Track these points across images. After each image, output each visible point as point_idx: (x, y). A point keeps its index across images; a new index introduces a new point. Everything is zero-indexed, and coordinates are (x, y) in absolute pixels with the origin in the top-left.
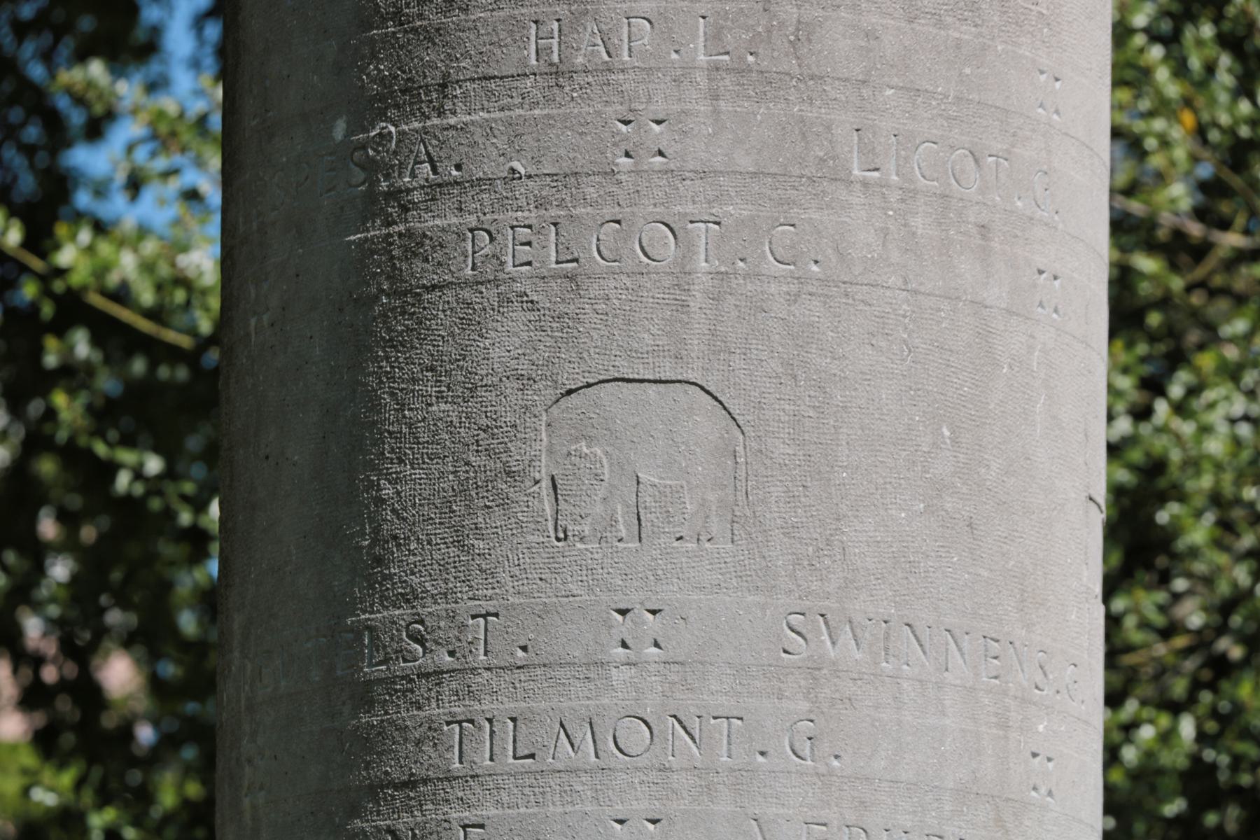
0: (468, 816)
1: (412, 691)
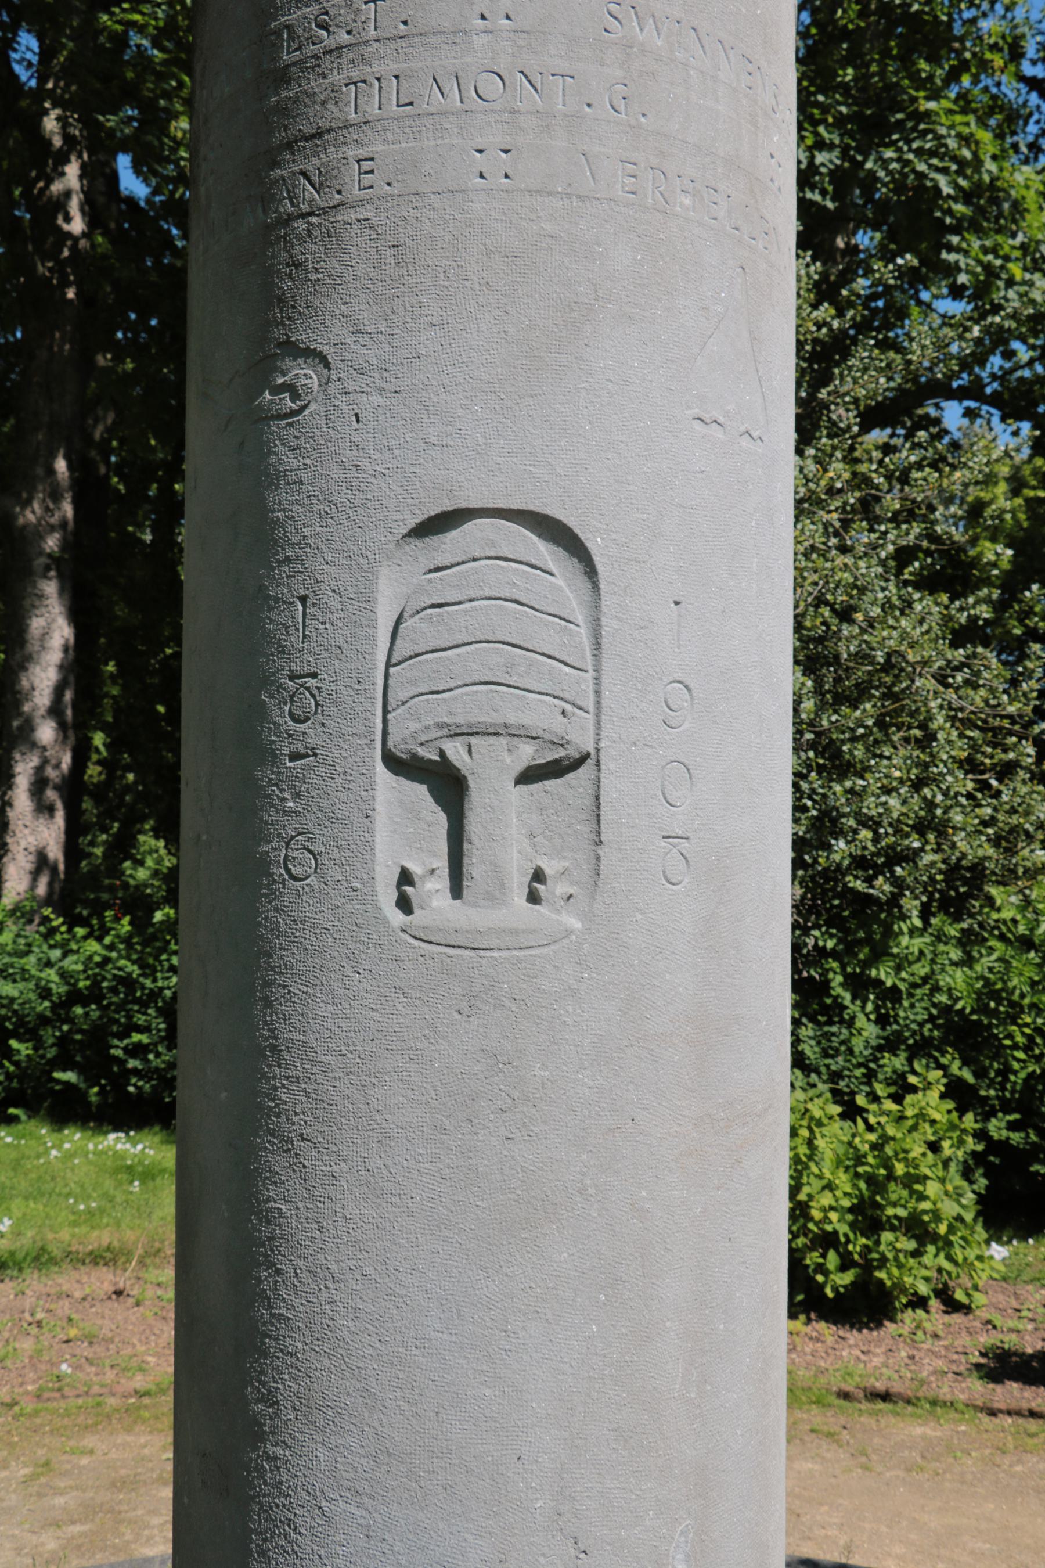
0: (362, 153)
1: (319, 66)
